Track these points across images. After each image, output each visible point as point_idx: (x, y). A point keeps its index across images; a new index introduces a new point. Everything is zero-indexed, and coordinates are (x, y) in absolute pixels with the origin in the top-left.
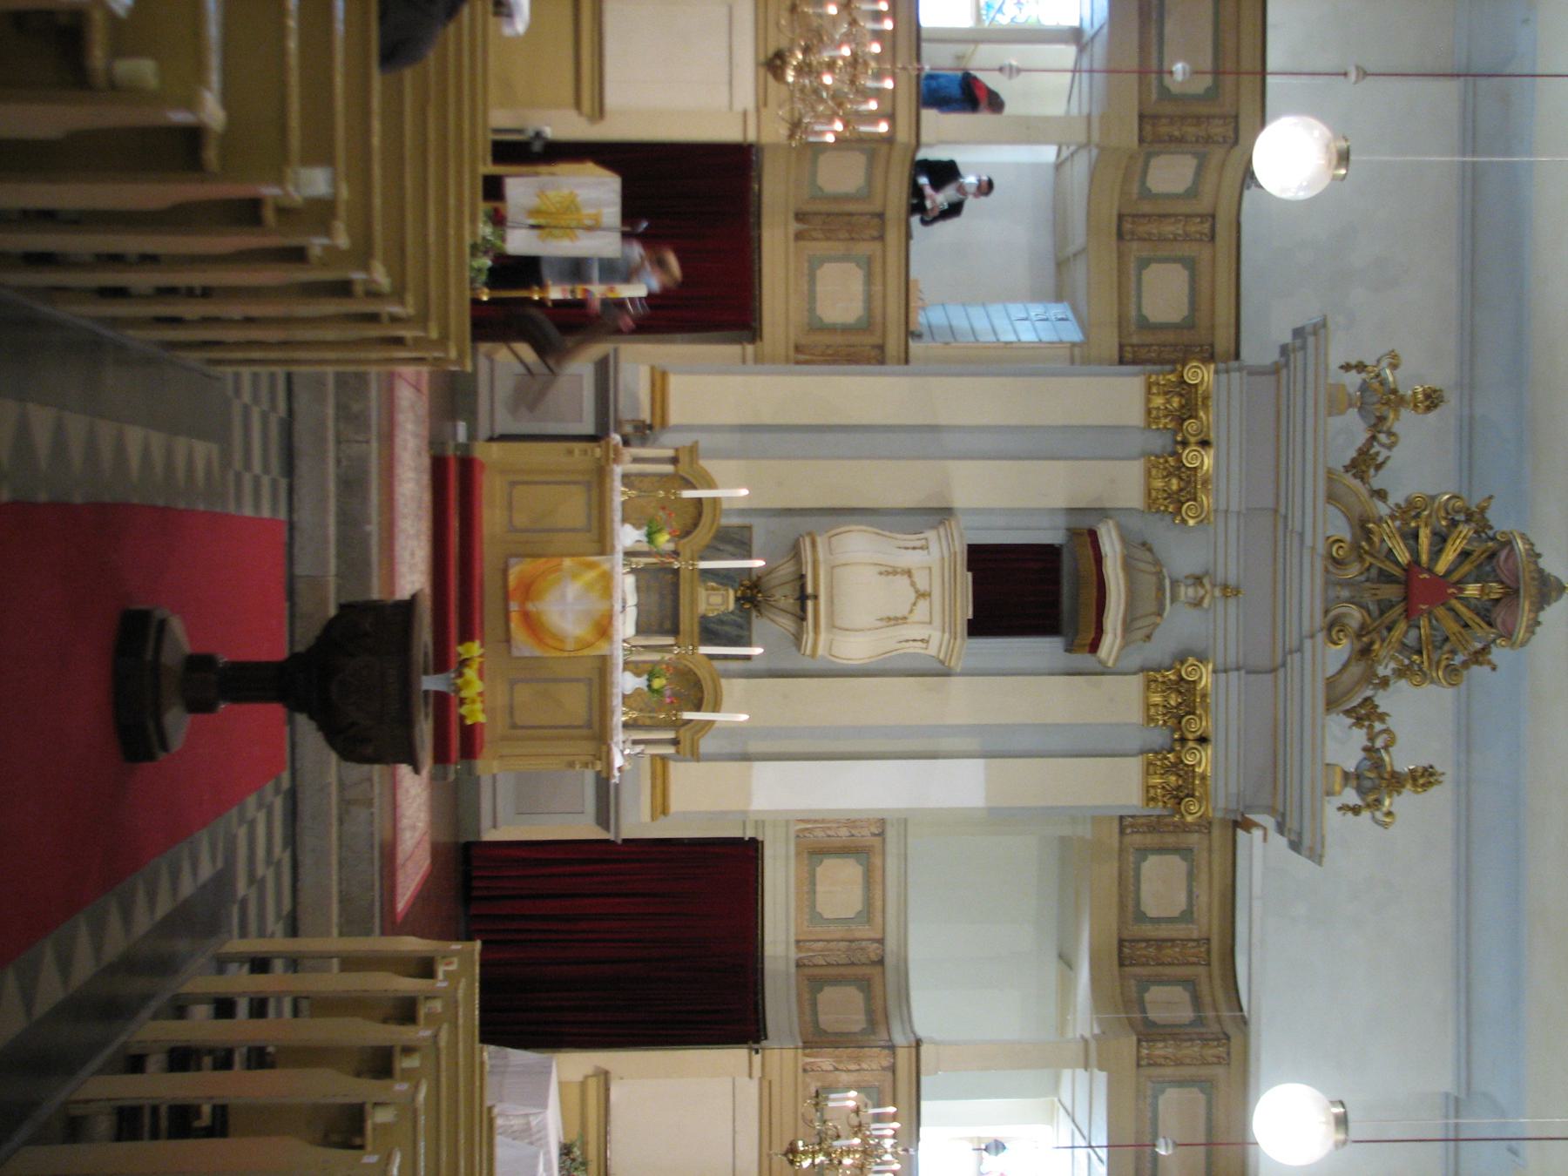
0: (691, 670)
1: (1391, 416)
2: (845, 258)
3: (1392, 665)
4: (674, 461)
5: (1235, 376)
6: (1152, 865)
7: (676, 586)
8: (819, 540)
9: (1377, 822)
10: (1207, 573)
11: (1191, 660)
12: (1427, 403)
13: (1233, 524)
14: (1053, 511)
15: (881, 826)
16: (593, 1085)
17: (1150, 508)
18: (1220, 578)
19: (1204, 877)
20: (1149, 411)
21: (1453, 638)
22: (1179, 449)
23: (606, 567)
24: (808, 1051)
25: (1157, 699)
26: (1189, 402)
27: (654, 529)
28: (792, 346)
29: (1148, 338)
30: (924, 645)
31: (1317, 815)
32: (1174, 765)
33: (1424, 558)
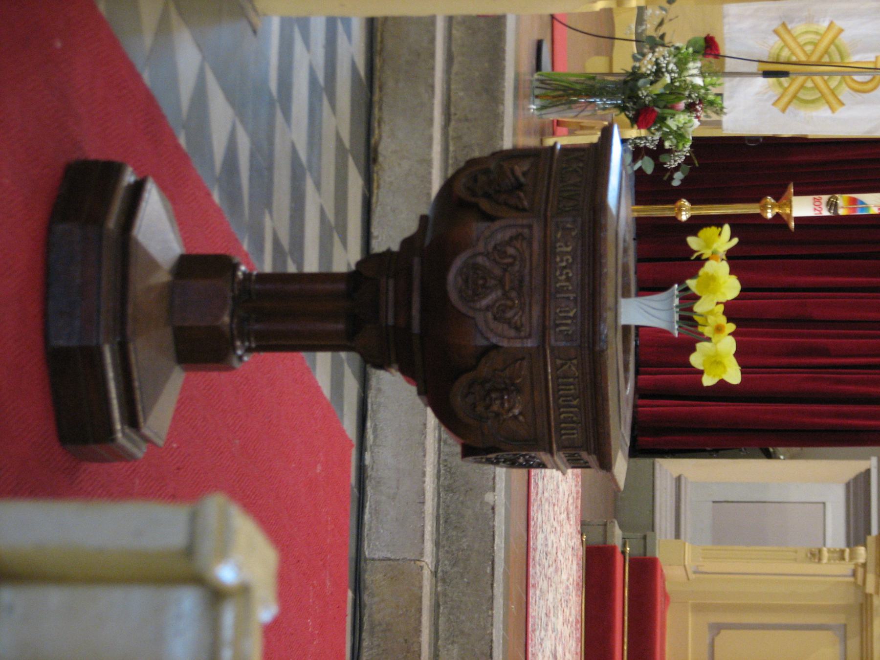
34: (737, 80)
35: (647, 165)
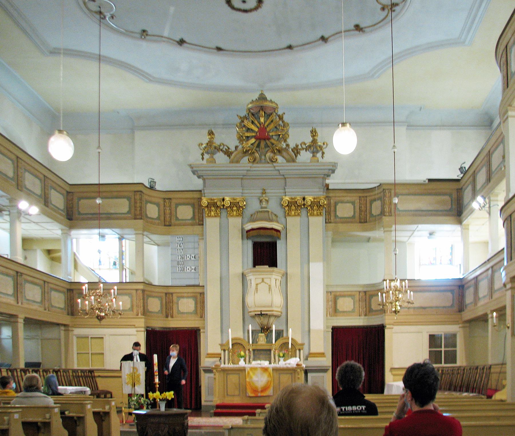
0: (280, 346)
1: (214, 145)
2: (178, 304)
3: (283, 143)
4: (224, 350)
5: (205, 191)
6: (339, 214)
7: (258, 350)
8: (250, 310)
9: (326, 147)
10: (259, 199)
11: (282, 203)
12: (211, 134)
13: (246, 191)
14: (243, 244)
15: (329, 293)
16: (394, 372)
17: (241, 216)
18: (260, 195)
19: (343, 198)
20: (215, 216)
21: (275, 125)
22: (225, 207)
23: (249, 369)
24: (386, 312)
25: (293, 213)
26: (212, 204)
27: (240, 356)
28: (200, 319)
29: (197, 217)
30: (277, 280)
31: (324, 164)
32: (311, 207)
33: (254, 134)
34: (136, 391)
35: (150, 407)
